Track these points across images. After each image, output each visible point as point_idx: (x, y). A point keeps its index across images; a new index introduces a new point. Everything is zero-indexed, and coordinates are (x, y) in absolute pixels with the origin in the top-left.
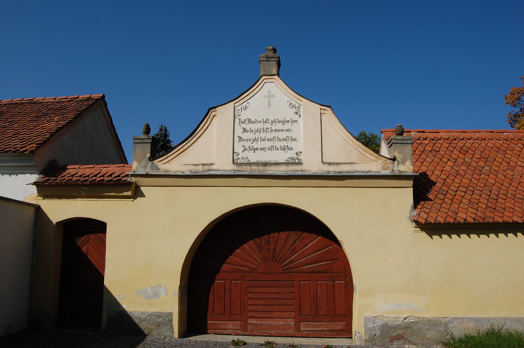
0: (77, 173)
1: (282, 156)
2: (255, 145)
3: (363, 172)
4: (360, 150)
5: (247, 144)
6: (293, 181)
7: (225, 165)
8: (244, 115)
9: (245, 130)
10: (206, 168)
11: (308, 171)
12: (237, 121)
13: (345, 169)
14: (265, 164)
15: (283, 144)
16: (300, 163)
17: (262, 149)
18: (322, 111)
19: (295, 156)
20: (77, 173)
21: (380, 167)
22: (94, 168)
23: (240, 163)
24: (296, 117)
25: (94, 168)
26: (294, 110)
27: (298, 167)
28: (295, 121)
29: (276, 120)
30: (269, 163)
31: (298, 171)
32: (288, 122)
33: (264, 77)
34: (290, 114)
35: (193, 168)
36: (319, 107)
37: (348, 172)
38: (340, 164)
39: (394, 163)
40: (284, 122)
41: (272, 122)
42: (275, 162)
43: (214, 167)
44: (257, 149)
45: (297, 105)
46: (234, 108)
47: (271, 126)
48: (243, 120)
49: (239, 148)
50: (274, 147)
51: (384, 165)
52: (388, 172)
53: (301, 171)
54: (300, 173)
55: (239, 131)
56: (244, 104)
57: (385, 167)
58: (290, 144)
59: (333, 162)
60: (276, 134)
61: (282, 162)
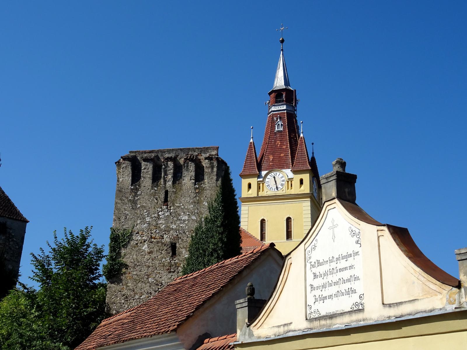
0: (215, 347)
1: (345, 304)
2: (326, 293)
3: (425, 312)
4: (422, 279)
5: (317, 293)
6: (404, 329)
7: (300, 325)
8: (315, 256)
9: (315, 276)
10: (286, 328)
11: (370, 319)
12: (308, 265)
13: (406, 311)
14: (332, 316)
15: (347, 286)
16: (361, 311)
17: (330, 297)
18: (380, 233)
19: (359, 301)
20: (215, 347)
21: (445, 301)
22: (226, 338)
23: (313, 318)
24: (357, 248)
25: (226, 338)
26: (355, 239)
27: (360, 316)
28: (357, 253)
29: (340, 256)
30: (336, 314)
31: (361, 321)
32: (350, 255)
33: (326, 204)
34: (351, 246)
35: (276, 330)
36: (376, 228)
37: (410, 314)
38: (401, 303)
39: (460, 292)
40: (347, 257)
41: (338, 259)
42: (341, 312)
43: (292, 327)
44: (325, 298)
45: (357, 231)
46: (305, 250)
47: (337, 265)
48: (313, 263)
49: (311, 301)
50: (340, 292)
51: (450, 297)
52: (450, 308)
53: (364, 320)
54: (362, 324)
55: (310, 279)
56: (313, 244)
57: (451, 299)
58: (354, 285)
59: (392, 303)
60: (341, 275)
61: (347, 310)
